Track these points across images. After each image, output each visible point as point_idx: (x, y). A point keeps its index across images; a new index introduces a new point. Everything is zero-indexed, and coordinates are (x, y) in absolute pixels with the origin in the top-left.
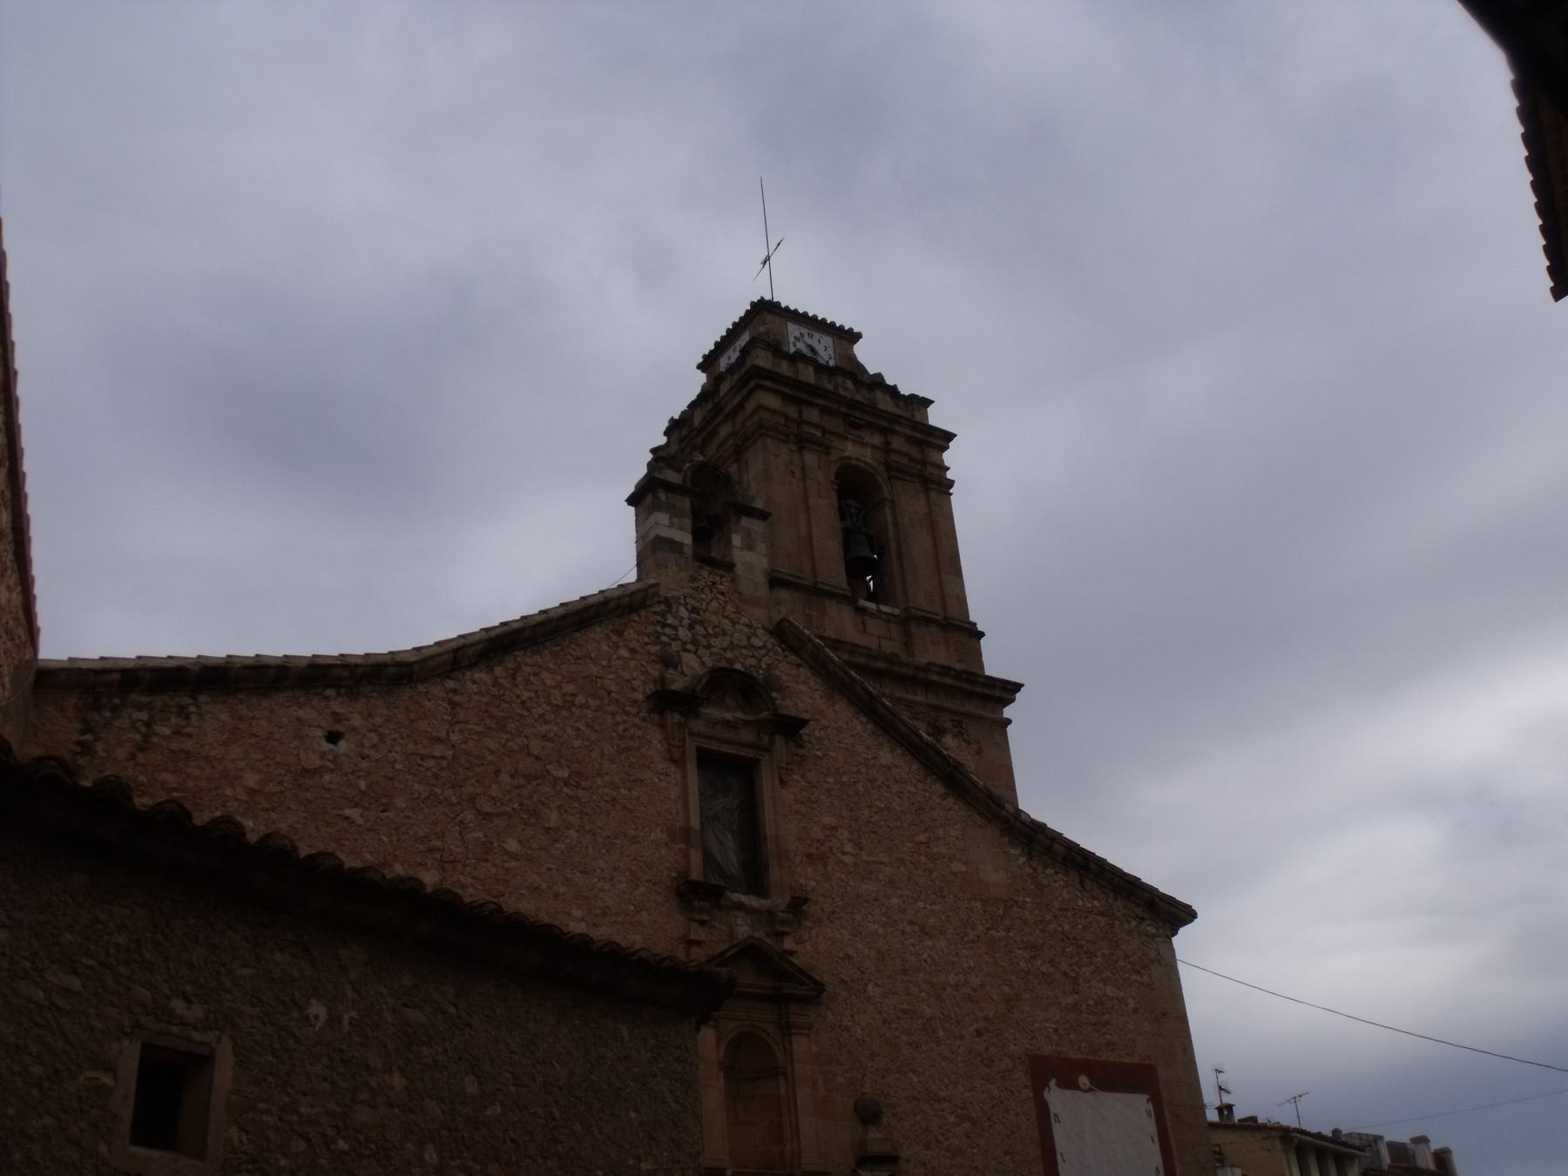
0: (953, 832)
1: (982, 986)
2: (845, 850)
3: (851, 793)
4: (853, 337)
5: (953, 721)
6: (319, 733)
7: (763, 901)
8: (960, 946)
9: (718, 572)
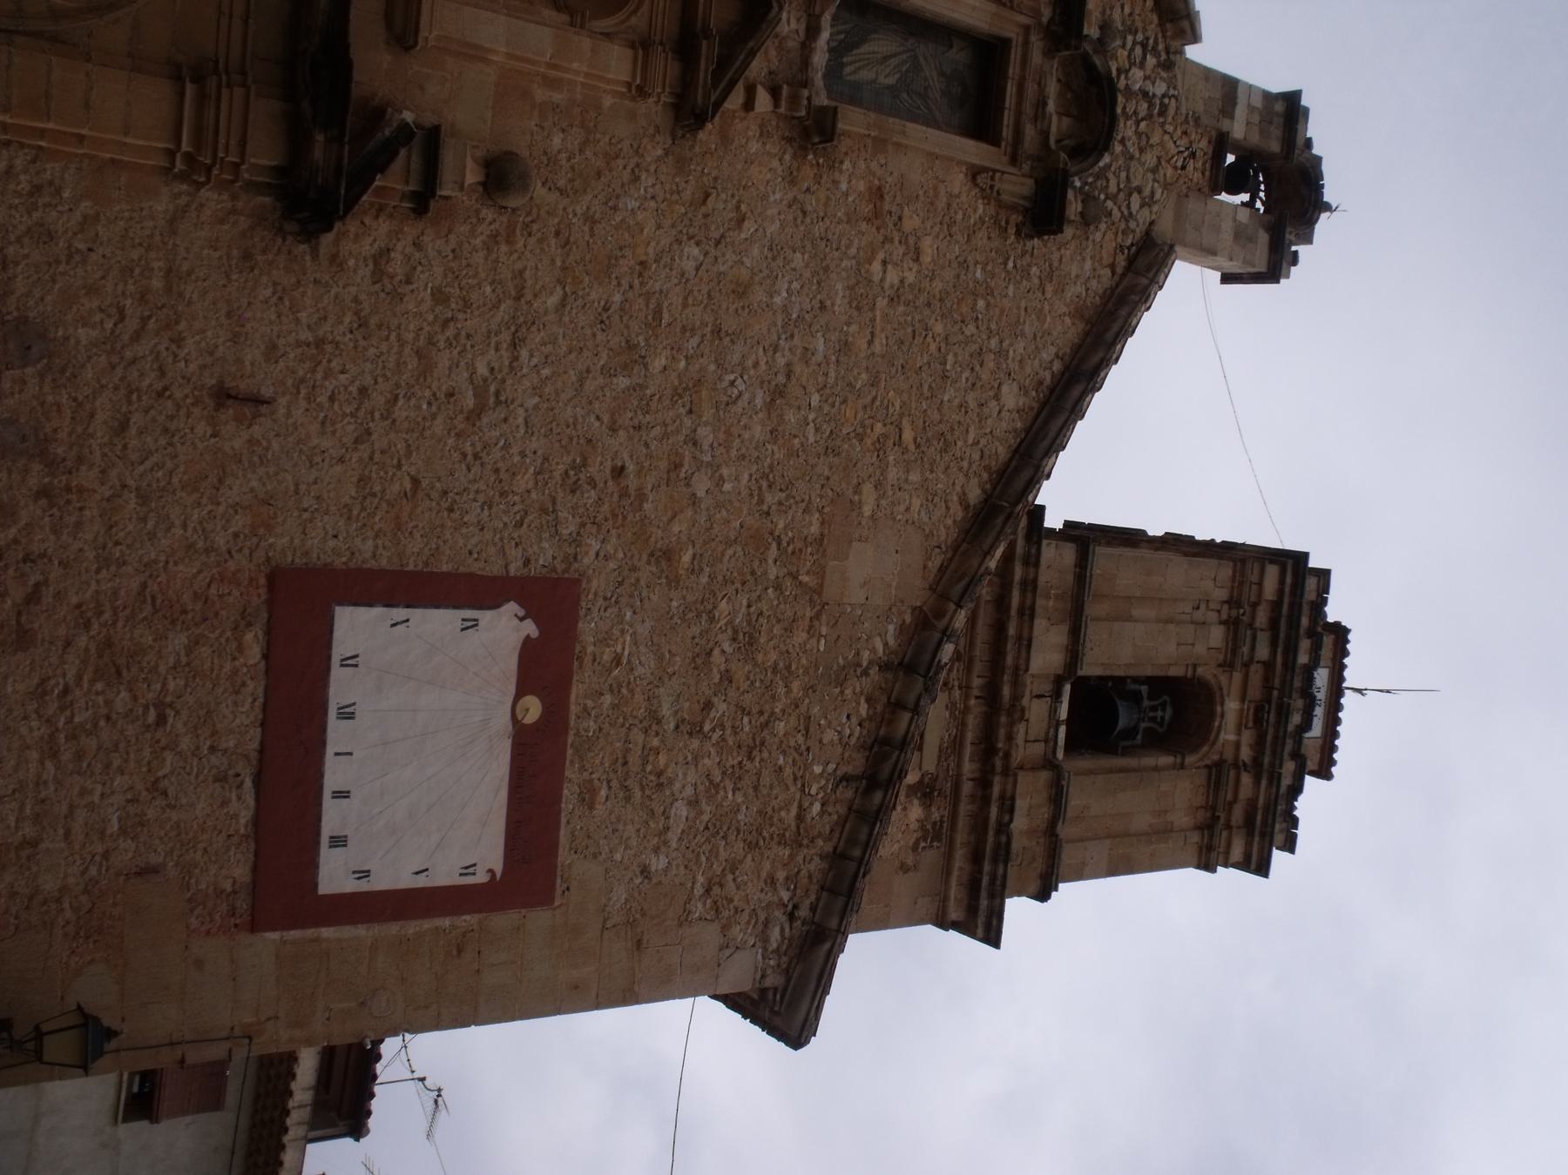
0: (916, 502)
1: (694, 500)
2: (889, 267)
3: (964, 309)
4: (1324, 772)
5: (942, 822)
7: (820, 74)
8: (755, 468)
9: (1208, 166)
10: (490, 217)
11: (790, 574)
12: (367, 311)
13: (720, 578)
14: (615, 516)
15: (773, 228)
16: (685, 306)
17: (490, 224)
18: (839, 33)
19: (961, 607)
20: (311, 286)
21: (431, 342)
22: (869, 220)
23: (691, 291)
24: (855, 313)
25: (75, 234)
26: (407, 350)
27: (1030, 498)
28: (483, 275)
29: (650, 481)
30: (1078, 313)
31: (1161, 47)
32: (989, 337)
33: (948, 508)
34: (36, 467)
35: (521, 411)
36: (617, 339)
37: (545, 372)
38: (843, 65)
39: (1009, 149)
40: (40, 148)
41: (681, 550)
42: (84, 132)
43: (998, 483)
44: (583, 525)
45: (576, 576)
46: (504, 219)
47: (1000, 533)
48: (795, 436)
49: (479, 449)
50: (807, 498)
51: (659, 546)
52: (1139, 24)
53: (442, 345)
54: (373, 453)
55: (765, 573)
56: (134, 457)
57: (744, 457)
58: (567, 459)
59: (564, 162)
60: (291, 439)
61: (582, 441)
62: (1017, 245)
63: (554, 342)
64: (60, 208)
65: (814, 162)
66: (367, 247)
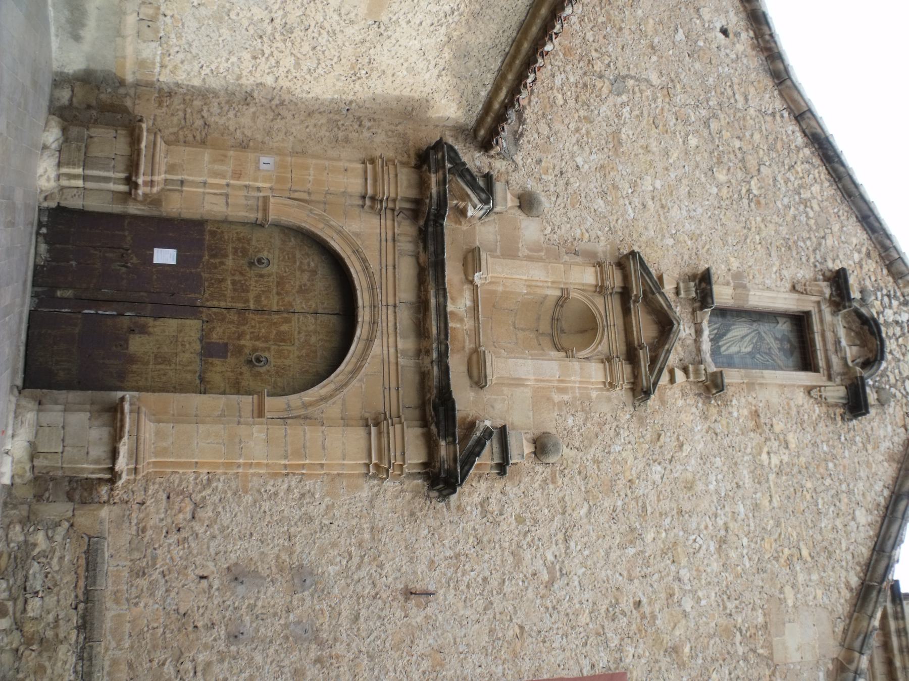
0: (819, 593)
1: (685, 614)
2: (772, 455)
3: (822, 470)
6: (724, 23)
7: (708, 355)
8: (717, 588)
10: (541, 470)
11: (751, 650)
12: (481, 534)
13: (709, 659)
14: (640, 631)
15: (700, 446)
16: (659, 501)
18: (714, 329)
19: (863, 654)
21: (519, 546)
23: (661, 492)
24: (758, 486)
26: (506, 553)
27: (890, 577)
28: (542, 503)
29: (657, 607)
30: (891, 458)
31: (899, 294)
33: (839, 592)
34: (313, 646)
35: (575, 578)
36: (624, 527)
37: (586, 553)
38: (719, 347)
39: (826, 373)
40: (303, 474)
41: (683, 645)
42: (323, 462)
43: (867, 571)
44: (622, 639)
45: (623, 670)
46: (549, 470)
47: (876, 602)
48: (738, 565)
52: (882, 285)
53: (525, 547)
54: (495, 614)
55: (736, 652)
56: (364, 634)
57: (710, 583)
58: (607, 602)
59: (576, 432)
60: (448, 613)
61: (614, 590)
63: (588, 534)
66: (476, 499)
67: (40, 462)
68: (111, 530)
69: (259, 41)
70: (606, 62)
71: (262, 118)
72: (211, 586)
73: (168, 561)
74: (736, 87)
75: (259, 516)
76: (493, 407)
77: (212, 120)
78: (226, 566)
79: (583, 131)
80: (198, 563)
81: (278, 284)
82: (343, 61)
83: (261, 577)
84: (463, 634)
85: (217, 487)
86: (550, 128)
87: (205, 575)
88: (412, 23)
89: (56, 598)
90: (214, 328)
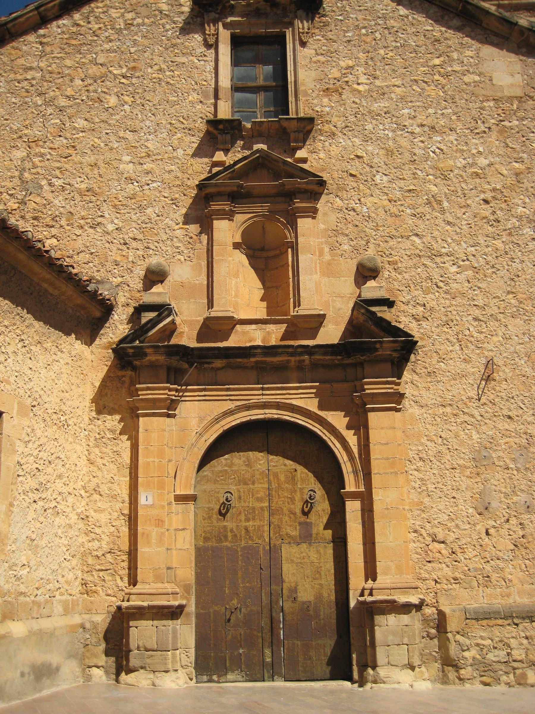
1: (491, 165)
2: (359, 81)
10: (388, 273)
13: (523, 148)
16: (404, 179)
17: (390, 272)
20: (436, 347)
22: (340, 94)
24: (386, 96)
25: (435, 443)
32: (379, 25)
41: (514, 168)
43: (448, 10)
49: (489, 267)
50: (478, 110)
51: (515, 179)
54: (500, 313)
61: (476, 219)
62: (330, 16)
64: (427, 450)
65: (321, 125)
67: (416, 661)
68: (457, 603)
69: (48, 511)
70: (8, 197)
71: (99, 504)
72: (494, 527)
73: (477, 560)
74: (19, 77)
75: (439, 492)
76: (339, 309)
77: (106, 547)
78: (478, 516)
79: (82, 222)
80: (477, 537)
81: (246, 484)
82: (57, 437)
83: (484, 489)
84: (516, 338)
85: (419, 525)
86: (82, 252)
87: (485, 531)
88: (31, 376)
89: (511, 640)
90: (287, 534)
